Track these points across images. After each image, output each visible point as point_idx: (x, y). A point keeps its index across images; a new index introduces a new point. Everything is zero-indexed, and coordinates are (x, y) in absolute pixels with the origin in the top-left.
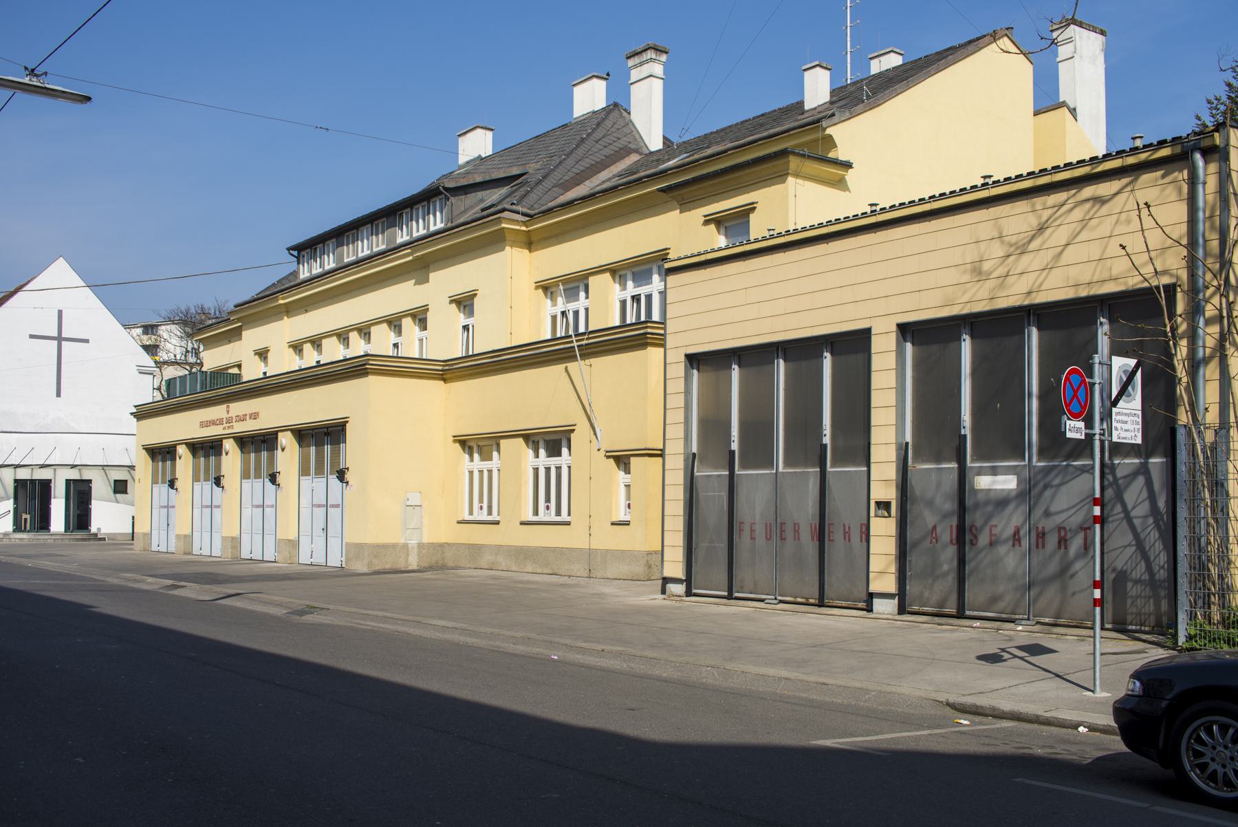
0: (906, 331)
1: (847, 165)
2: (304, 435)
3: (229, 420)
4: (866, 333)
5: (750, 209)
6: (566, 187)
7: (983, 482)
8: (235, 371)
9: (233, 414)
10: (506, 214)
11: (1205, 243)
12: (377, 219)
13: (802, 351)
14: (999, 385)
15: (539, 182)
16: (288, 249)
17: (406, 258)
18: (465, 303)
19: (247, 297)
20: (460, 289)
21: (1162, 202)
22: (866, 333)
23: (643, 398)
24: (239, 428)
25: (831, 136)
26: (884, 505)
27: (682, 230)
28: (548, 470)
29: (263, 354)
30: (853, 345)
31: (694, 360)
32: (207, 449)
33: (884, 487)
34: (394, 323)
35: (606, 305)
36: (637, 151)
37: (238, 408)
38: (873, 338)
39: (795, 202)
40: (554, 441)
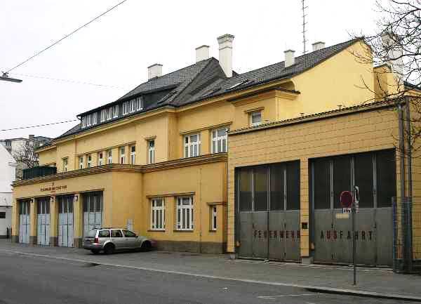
0: (311, 161)
1: (298, 93)
2: (85, 195)
3: (54, 189)
4: (298, 161)
5: (260, 110)
6: (193, 93)
7: (339, 216)
8: (52, 166)
9: (55, 186)
10: (168, 106)
11: (407, 134)
12: (132, 99)
13: (276, 168)
14: (342, 182)
15: (181, 92)
16: (78, 116)
17: (126, 121)
18: (151, 142)
19: (59, 135)
20: (149, 135)
21: (390, 120)
22: (298, 161)
23: (211, 185)
24: (58, 192)
25: (292, 82)
26: (304, 225)
27: (236, 116)
28: (184, 210)
29: (65, 160)
30: (296, 163)
31: (238, 170)
32: (42, 202)
33: (305, 218)
34: (121, 148)
35: (201, 146)
36: (221, 78)
37: (58, 183)
38: (301, 163)
39: (281, 109)
40: (185, 198)
